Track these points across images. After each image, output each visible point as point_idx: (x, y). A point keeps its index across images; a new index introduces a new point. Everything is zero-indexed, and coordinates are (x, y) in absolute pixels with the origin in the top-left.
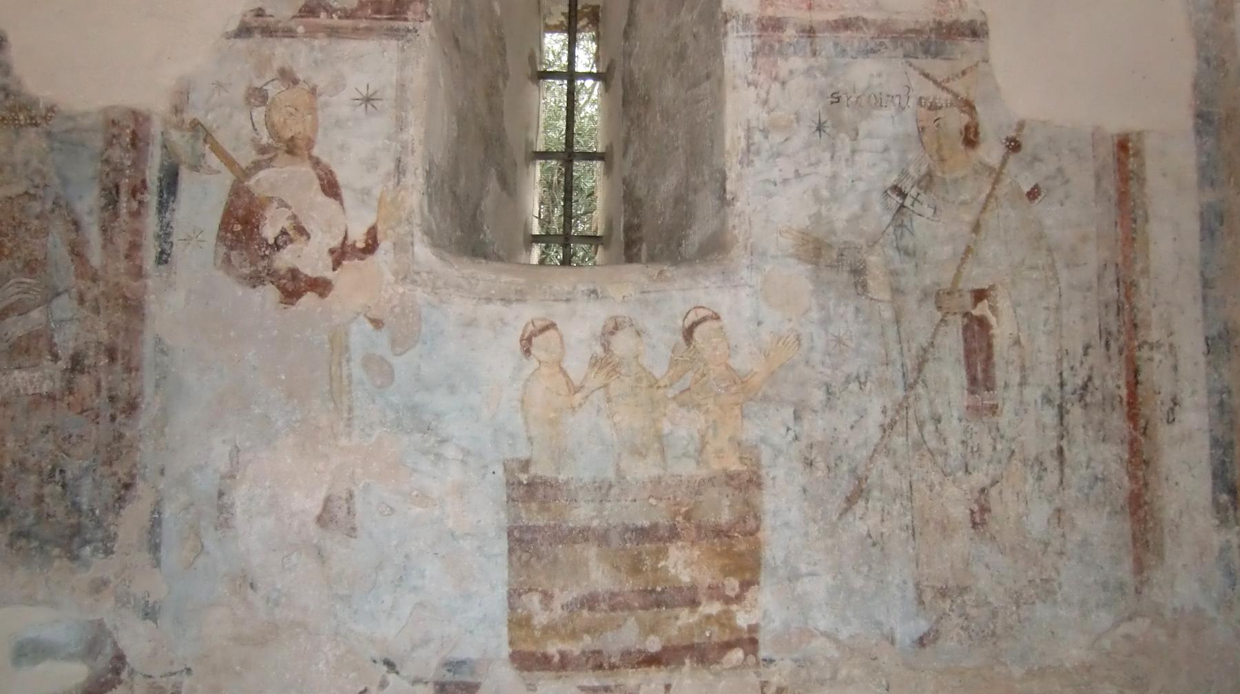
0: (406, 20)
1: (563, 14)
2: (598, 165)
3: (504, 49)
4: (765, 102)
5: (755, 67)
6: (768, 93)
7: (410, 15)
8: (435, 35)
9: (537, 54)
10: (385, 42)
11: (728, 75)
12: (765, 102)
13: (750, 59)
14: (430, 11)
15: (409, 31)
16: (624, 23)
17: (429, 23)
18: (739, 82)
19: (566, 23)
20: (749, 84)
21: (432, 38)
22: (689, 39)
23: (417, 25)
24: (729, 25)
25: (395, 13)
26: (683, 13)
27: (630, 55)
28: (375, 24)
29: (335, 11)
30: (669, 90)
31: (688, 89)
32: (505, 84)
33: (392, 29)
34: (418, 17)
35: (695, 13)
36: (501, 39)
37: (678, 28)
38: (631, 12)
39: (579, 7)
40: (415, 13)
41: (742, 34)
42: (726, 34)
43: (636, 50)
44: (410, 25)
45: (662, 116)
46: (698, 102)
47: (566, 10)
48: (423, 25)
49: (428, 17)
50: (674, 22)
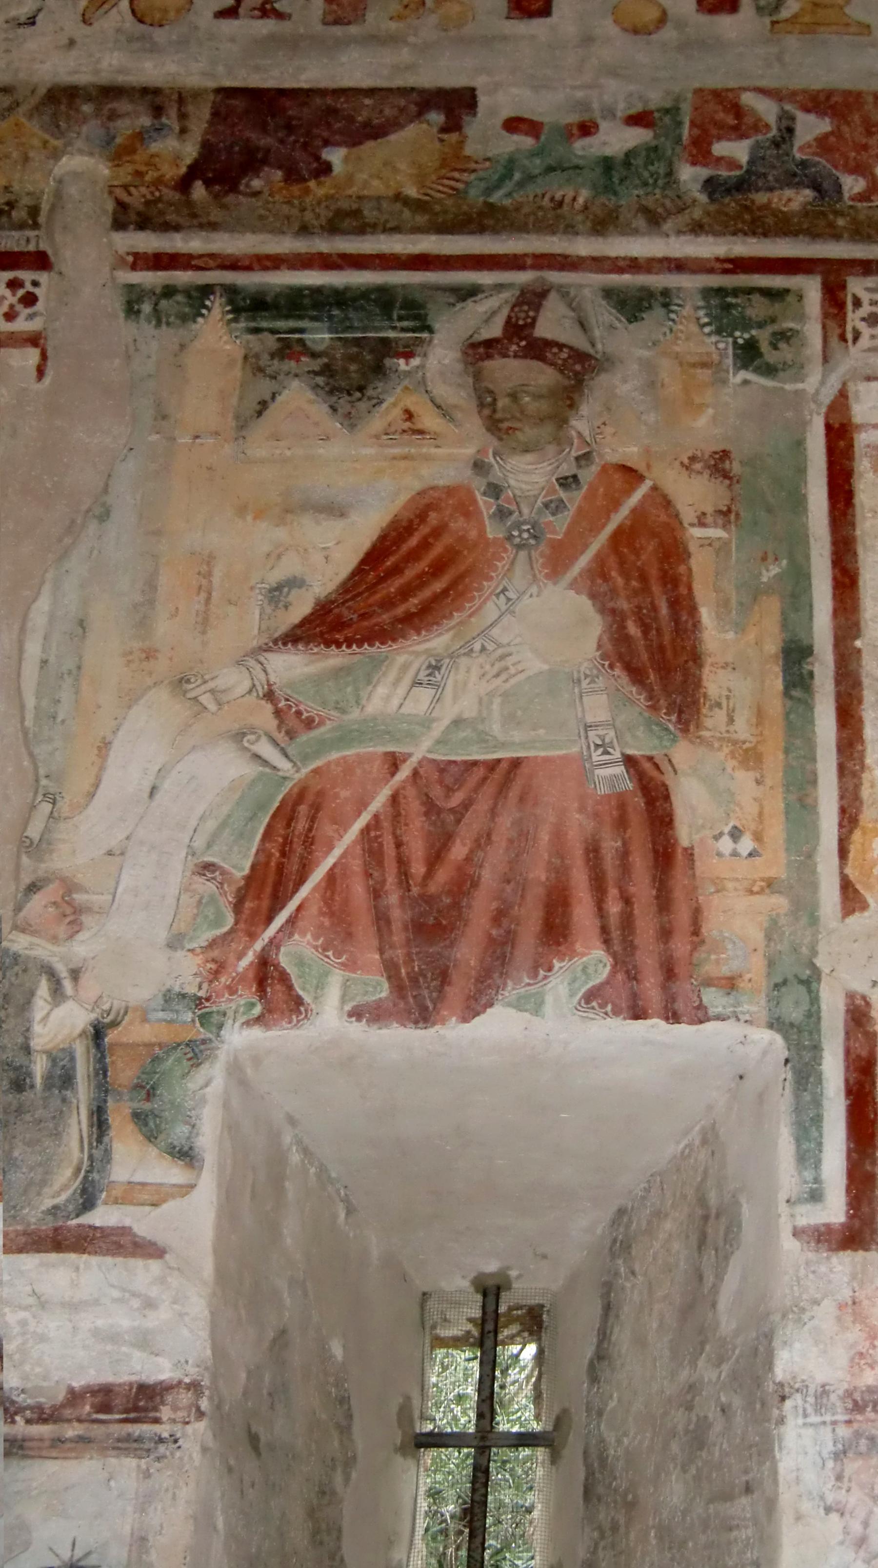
0: (157, 1421)
1: (470, 1320)
2: (541, 1453)
3: (349, 1416)
4: (861, 1542)
5: (839, 1478)
6: (866, 1524)
7: (165, 1413)
8: (211, 1443)
9: (416, 1402)
10: (113, 1461)
11: (786, 1497)
12: (861, 1542)
13: (830, 1464)
14: (204, 1404)
15: (161, 1440)
16: (589, 1352)
17: (201, 1426)
18: (806, 1506)
19: (476, 1333)
20: (828, 1510)
21: (205, 1450)
22: (713, 1413)
23: (178, 1429)
24: (788, 1404)
25: (136, 1409)
26: (701, 1363)
27: (600, 1413)
28: (97, 1431)
29: (20, 1410)
30: (674, 1491)
31: (711, 1501)
32: (347, 1479)
33: (128, 1438)
34: (180, 1414)
35: (726, 1368)
36: (344, 1400)
37: (692, 1388)
38: (603, 1335)
39: (502, 1309)
40: (175, 1409)
41: (814, 1419)
42: (781, 1421)
43: (612, 1404)
44: (164, 1430)
45: (660, 1538)
46: (731, 1529)
47: (477, 1313)
48: (189, 1428)
49: (200, 1414)
50: (684, 1375)
